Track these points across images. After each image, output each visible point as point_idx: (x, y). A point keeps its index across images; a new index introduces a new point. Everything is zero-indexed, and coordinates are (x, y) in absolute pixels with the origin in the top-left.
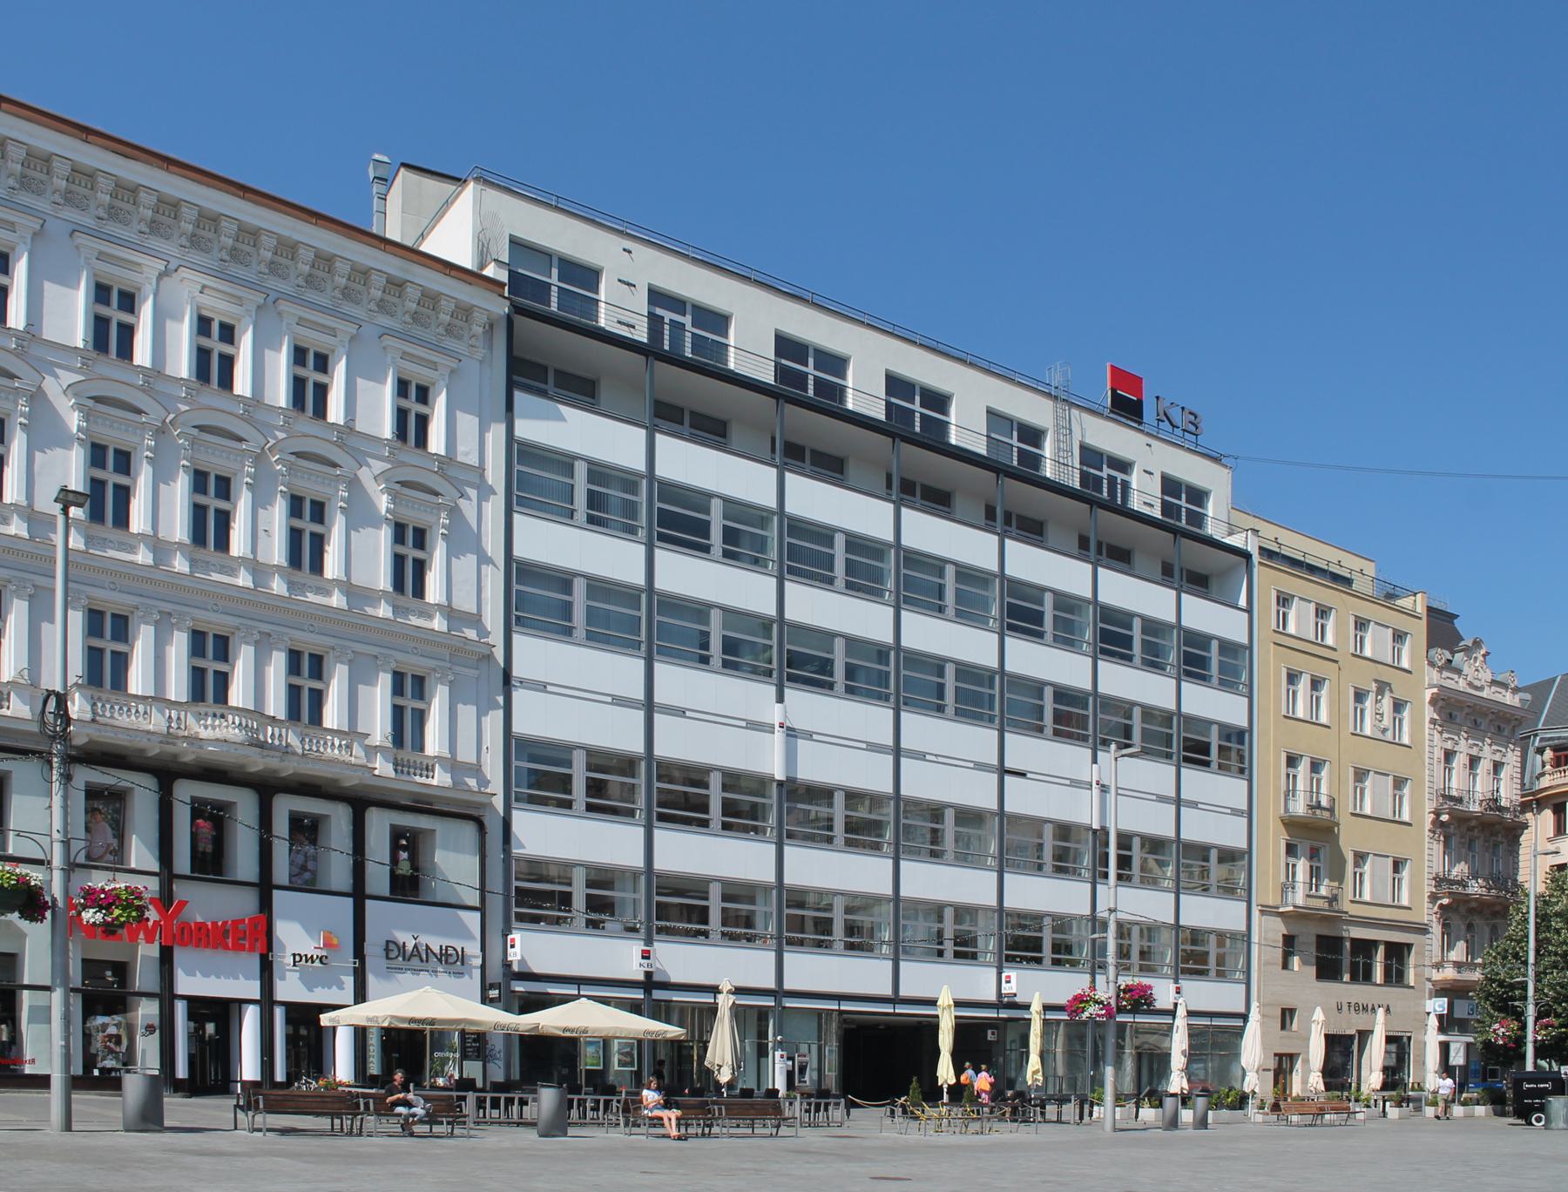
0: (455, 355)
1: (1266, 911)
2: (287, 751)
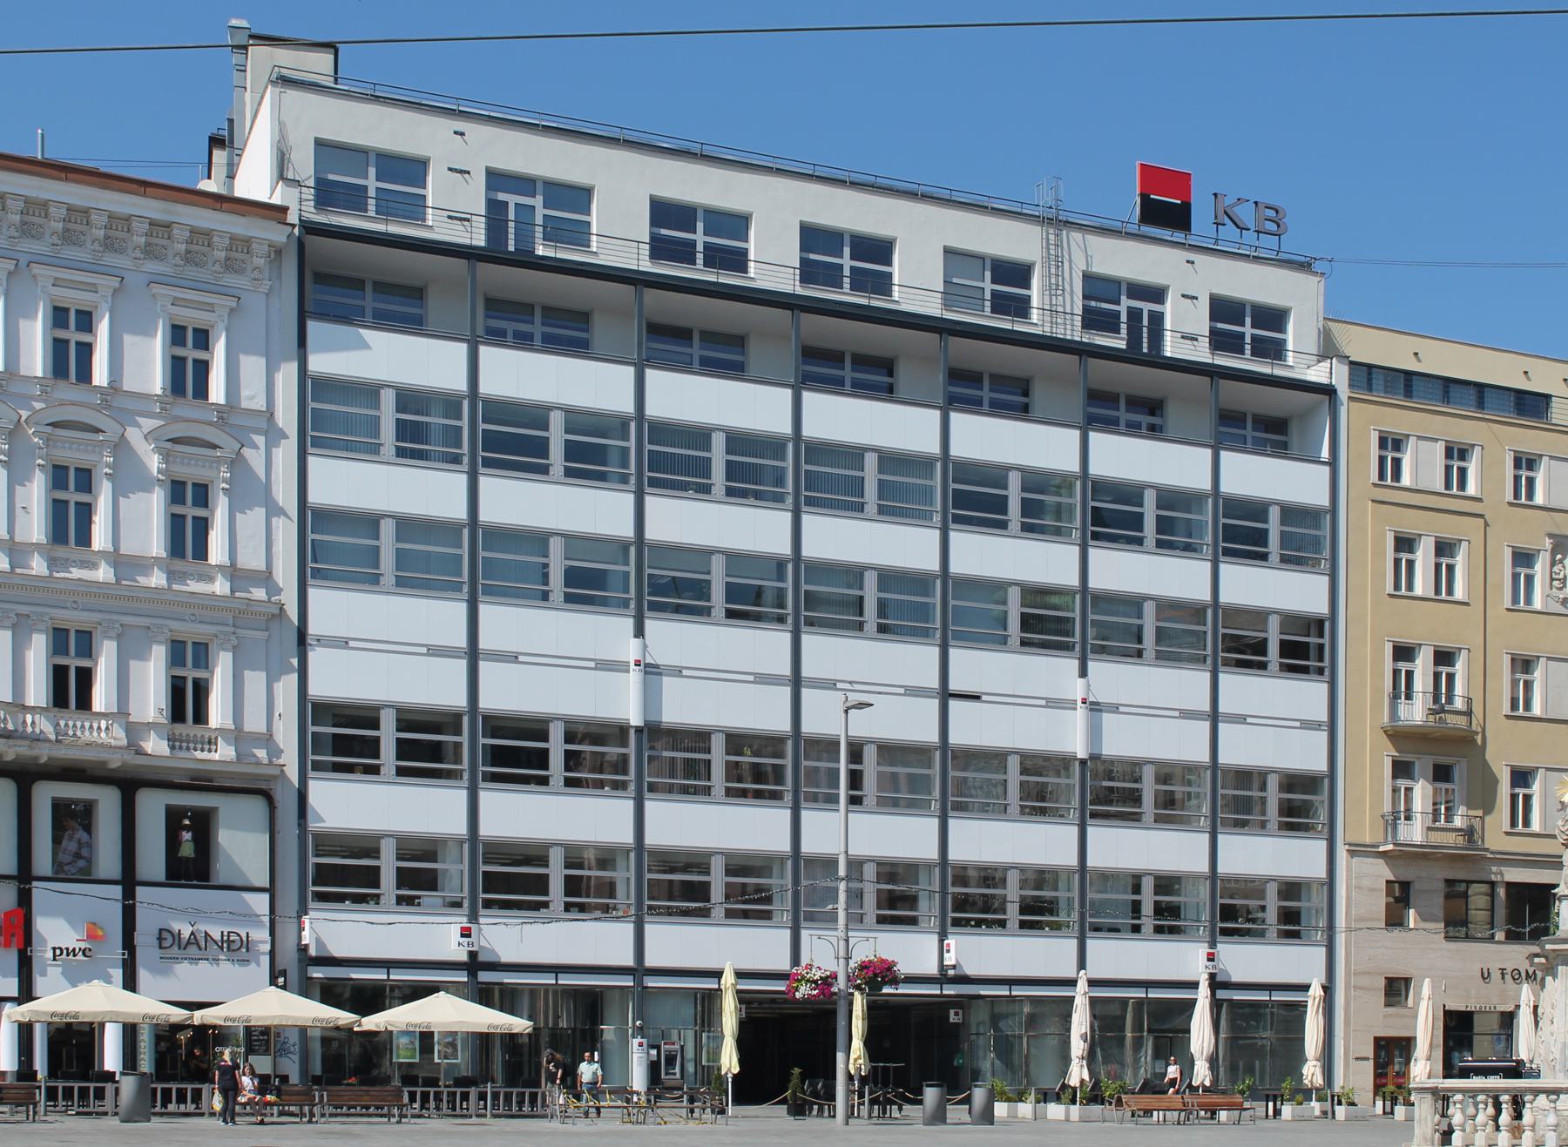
0: (230, 291)
2: (38, 739)
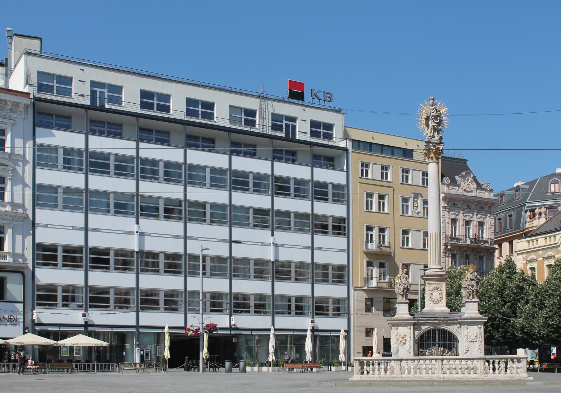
1: (356, 289)
